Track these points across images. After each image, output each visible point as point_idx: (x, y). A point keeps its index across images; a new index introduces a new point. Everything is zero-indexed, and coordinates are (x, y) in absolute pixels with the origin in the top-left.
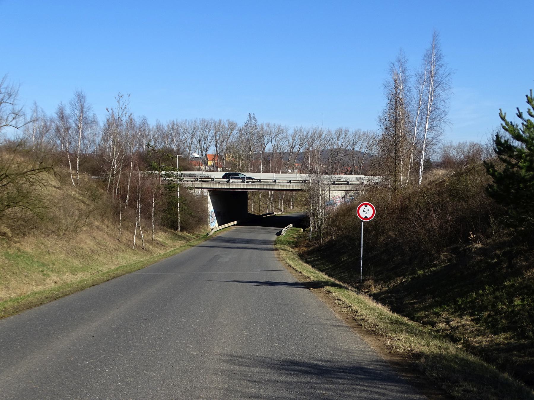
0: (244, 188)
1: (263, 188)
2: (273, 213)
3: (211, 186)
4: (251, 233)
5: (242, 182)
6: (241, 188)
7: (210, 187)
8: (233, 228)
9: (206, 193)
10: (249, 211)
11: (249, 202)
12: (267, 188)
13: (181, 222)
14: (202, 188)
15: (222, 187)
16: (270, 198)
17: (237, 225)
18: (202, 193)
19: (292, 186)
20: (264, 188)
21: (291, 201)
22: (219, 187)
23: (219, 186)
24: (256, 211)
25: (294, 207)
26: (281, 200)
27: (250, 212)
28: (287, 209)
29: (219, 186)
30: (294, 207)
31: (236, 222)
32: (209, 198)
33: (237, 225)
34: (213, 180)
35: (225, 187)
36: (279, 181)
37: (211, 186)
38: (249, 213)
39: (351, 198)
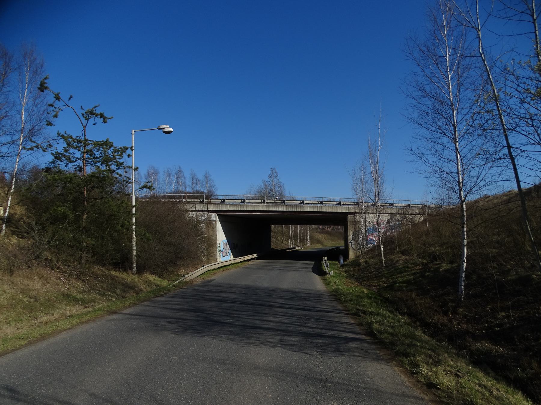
0: (264, 210)
1: (288, 210)
2: (295, 248)
3: (221, 208)
4: (273, 270)
5: (261, 203)
6: (260, 210)
7: (218, 209)
8: (251, 263)
9: (214, 217)
10: (273, 247)
11: (273, 239)
12: (294, 210)
13: (138, 255)
14: (208, 211)
15: (235, 209)
16: (291, 236)
17: (257, 258)
18: (209, 217)
19: (324, 208)
20: (290, 210)
21: (307, 240)
22: (231, 209)
23: (231, 207)
24: (279, 247)
25: (309, 244)
26: (300, 238)
27: (274, 247)
28: (305, 246)
29: (231, 207)
30: (309, 244)
31: (255, 256)
32: (219, 226)
33: (257, 258)
34: (224, 201)
35: (239, 209)
36: (308, 202)
37: (221, 208)
38: (273, 248)
39: (397, 223)
